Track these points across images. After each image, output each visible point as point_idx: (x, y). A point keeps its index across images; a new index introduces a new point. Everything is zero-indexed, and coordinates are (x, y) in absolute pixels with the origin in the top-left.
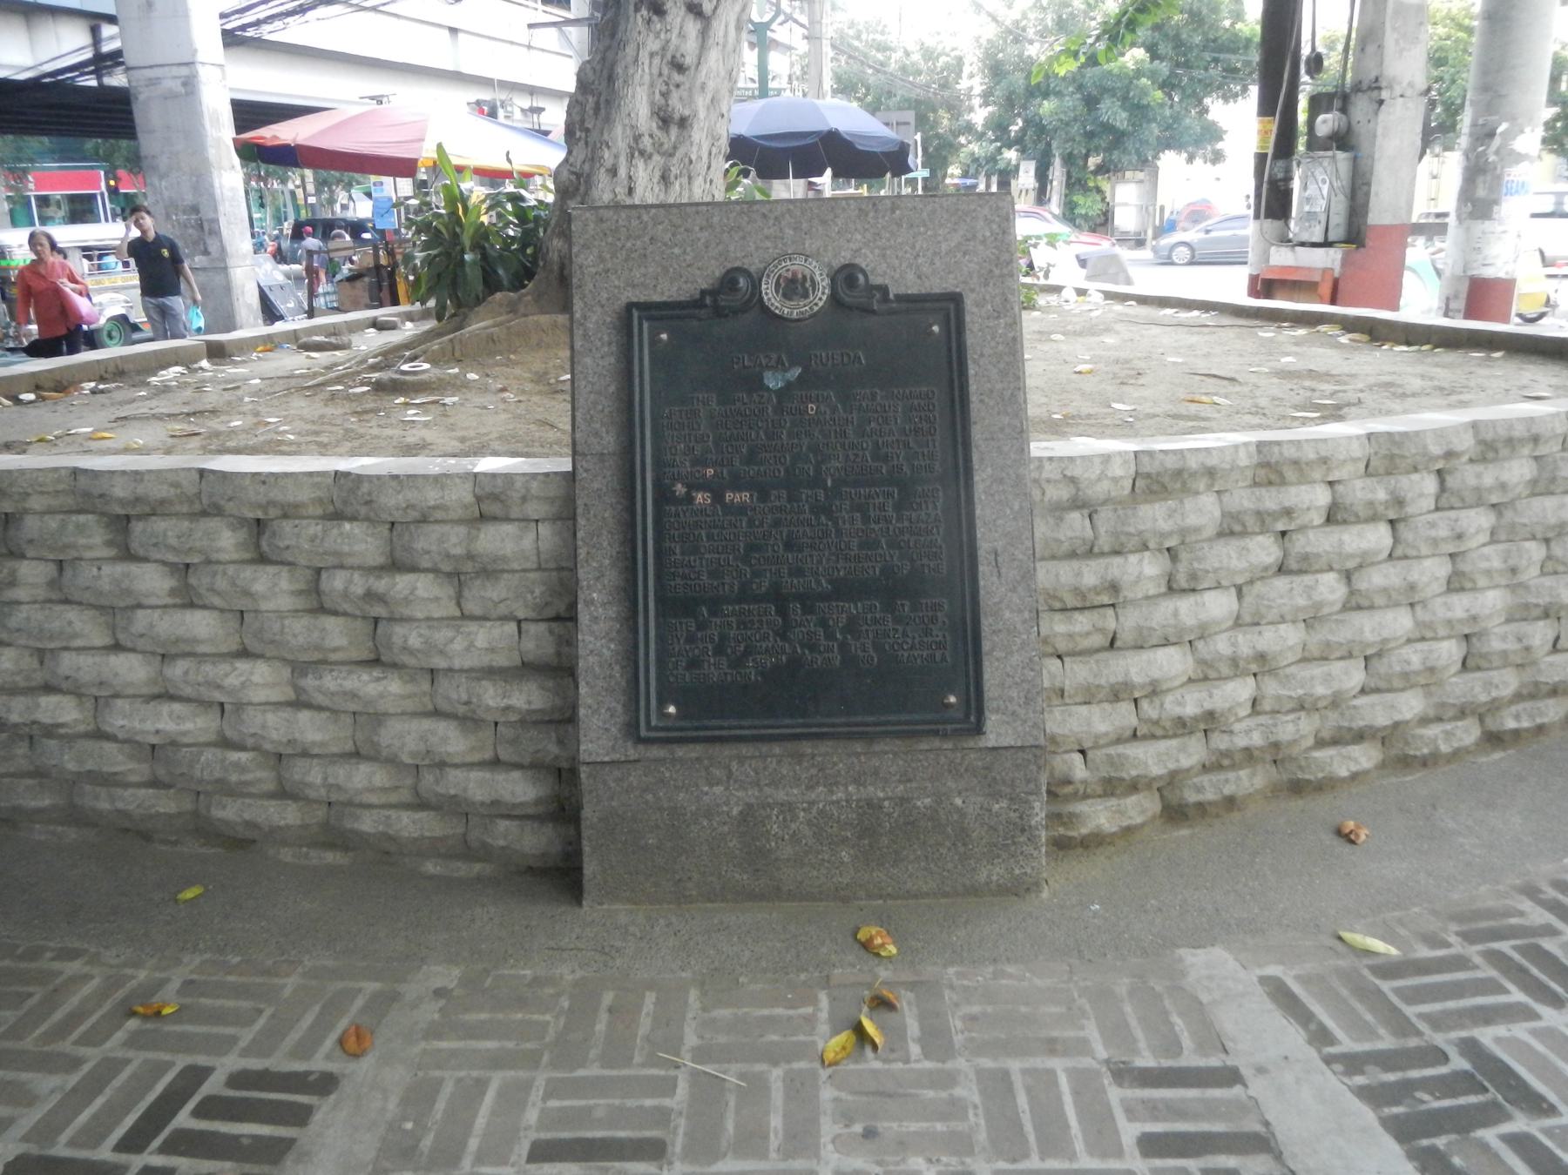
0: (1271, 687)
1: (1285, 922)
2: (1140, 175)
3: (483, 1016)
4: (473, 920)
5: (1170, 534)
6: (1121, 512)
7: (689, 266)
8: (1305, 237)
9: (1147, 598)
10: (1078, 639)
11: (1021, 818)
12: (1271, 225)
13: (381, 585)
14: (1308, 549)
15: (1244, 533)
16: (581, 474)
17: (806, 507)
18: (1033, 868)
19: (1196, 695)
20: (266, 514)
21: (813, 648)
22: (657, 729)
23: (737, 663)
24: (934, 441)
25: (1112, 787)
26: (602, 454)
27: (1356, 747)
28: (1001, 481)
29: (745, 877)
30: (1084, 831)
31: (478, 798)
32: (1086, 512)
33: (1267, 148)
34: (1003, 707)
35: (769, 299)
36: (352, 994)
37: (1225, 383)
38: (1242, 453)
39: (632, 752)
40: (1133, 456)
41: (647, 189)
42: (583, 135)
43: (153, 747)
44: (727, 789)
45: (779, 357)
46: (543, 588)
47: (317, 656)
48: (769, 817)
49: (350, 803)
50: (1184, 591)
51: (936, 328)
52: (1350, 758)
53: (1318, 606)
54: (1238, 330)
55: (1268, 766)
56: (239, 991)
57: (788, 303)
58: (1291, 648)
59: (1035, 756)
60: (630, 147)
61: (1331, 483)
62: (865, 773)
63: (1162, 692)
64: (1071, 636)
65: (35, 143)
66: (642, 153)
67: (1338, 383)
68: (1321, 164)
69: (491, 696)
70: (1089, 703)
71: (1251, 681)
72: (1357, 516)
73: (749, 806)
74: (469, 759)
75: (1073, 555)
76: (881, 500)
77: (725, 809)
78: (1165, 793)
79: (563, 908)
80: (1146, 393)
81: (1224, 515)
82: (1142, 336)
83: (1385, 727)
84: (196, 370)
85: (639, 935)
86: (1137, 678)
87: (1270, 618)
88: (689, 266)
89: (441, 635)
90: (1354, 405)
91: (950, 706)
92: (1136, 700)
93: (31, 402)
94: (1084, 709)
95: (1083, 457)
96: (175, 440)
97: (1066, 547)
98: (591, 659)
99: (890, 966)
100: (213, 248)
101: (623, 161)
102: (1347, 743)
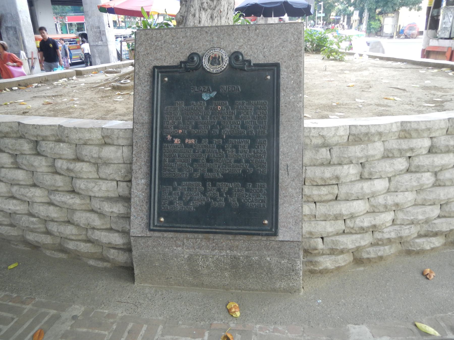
0: (401, 215)
1: (394, 315)
2: (393, 15)
3: (85, 330)
4: (96, 286)
5: (362, 158)
6: (342, 149)
7: (177, 52)
8: (443, 36)
9: (351, 182)
10: (322, 196)
11: (292, 266)
12: (431, 32)
13: (71, 166)
14: (419, 164)
15: (393, 157)
16: (135, 130)
17: (215, 146)
18: (297, 284)
19: (369, 219)
20: (37, 139)
21: (215, 199)
22: (156, 226)
24: (265, 121)
25: (333, 252)
26: (143, 123)
27: (434, 238)
28: (291, 138)
29: (191, 279)
30: (321, 268)
31: (104, 241)
32: (328, 149)
33: (431, 5)
36: (45, 314)
37: (402, 91)
38: (394, 126)
39: (149, 234)
40: (348, 127)
41: (205, 20)
42: (185, 3)
43: (10, 213)
44: (183, 248)
45: (209, 87)
46: (125, 170)
47: (54, 188)
48: (198, 259)
49: (66, 238)
50: (367, 179)
51: (269, 77)
52: (431, 242)
53: (422, 185)
54: (413, 70)
55: (397, 244)
56: (10, 309)
58: (409, 201)
59: (298, 245)
60: (200, 7)
61: (431, 138)
62: (233, 247)
63: (356, 217)
64: (320, 195)
65: (68, 8)
66: (204, 9)
67: (445, 92)
68: (450, 10)
69: (107, 208)
70: (326, 220)
71: (392, 213)
72: (441, 150)
73: (191, 255)
74: (102, 227)
75: (322, 165)
76: (244, 144)
77: (182, 255)
78: (355, 253)
79: (128, 284)
80: (371, 95)
81: (385, 150)
82: (377, 72)
83: (447, 231)
84: (70, 80)
85: (150, 298)
86: (344, 212)
87: (402, 189)
88: (177, 52)
89: (91, 185)
90: (449, 101)
91: (265, 224)
92: (345, 220)
93: (15, 90)
94: (323, 223)
95: (327, 128)
96: (43, 106)
97: (319, 162)
98: (136, 199)
99: (236, 322)
100: (104, 39)
101: (197, 11)
102: (431, 236)
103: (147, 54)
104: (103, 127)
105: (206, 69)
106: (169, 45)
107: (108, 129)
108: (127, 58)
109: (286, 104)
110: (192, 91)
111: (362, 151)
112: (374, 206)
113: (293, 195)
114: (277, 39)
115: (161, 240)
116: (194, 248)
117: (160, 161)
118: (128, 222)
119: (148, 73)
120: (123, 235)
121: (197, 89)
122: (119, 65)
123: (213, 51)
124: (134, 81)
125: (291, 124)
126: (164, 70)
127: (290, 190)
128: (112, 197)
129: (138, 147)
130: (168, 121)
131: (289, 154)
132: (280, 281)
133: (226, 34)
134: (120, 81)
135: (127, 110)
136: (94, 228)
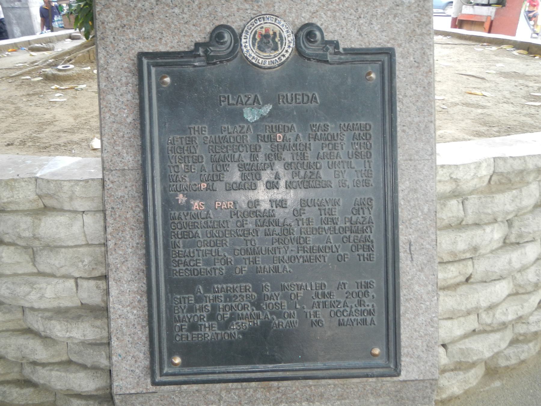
7: (186, 23)
16: (108, 183)
22: (167, 375)
23: (225, 326)
28: (415, 191)
31: (59, 387)
32: (460, 200)
34: (411, 353)
35: (248, 51)
37: (479, 80)
39: (152, 388)
40: (492, 160)
45: (256, 96)
46: (90, 259)
57: (262, 54)
62: (314, 396)
70: (452, 318)
76: (330, 207)
88: (186, 23)
89: (23, 290)
91: (375, 355)
95: (463, 165)
98: (120, 321)
103: (123, 27)
104: (38, 175)
105: (250, 58)
107: (48, 181)
108: (61, 26)
109: (405, 128)
110: (222, 103)
111: (513, 201)
112: (520, 286)
113: (421, 298)
115: (176, 396)
119: (128, 68)
120: (95, 374)
121: (233, 98)
122: (50, 38)
123: (262, 22)
124: (99, 82)
125: (415, 166)
126: (160, 61)
127: (417, 288)
128: (67, 307)
129: (118, 219)
130: (178, 166)
131: (412, 222)
134: (56, 65)
135: (75, 120)
136: (35, 363)
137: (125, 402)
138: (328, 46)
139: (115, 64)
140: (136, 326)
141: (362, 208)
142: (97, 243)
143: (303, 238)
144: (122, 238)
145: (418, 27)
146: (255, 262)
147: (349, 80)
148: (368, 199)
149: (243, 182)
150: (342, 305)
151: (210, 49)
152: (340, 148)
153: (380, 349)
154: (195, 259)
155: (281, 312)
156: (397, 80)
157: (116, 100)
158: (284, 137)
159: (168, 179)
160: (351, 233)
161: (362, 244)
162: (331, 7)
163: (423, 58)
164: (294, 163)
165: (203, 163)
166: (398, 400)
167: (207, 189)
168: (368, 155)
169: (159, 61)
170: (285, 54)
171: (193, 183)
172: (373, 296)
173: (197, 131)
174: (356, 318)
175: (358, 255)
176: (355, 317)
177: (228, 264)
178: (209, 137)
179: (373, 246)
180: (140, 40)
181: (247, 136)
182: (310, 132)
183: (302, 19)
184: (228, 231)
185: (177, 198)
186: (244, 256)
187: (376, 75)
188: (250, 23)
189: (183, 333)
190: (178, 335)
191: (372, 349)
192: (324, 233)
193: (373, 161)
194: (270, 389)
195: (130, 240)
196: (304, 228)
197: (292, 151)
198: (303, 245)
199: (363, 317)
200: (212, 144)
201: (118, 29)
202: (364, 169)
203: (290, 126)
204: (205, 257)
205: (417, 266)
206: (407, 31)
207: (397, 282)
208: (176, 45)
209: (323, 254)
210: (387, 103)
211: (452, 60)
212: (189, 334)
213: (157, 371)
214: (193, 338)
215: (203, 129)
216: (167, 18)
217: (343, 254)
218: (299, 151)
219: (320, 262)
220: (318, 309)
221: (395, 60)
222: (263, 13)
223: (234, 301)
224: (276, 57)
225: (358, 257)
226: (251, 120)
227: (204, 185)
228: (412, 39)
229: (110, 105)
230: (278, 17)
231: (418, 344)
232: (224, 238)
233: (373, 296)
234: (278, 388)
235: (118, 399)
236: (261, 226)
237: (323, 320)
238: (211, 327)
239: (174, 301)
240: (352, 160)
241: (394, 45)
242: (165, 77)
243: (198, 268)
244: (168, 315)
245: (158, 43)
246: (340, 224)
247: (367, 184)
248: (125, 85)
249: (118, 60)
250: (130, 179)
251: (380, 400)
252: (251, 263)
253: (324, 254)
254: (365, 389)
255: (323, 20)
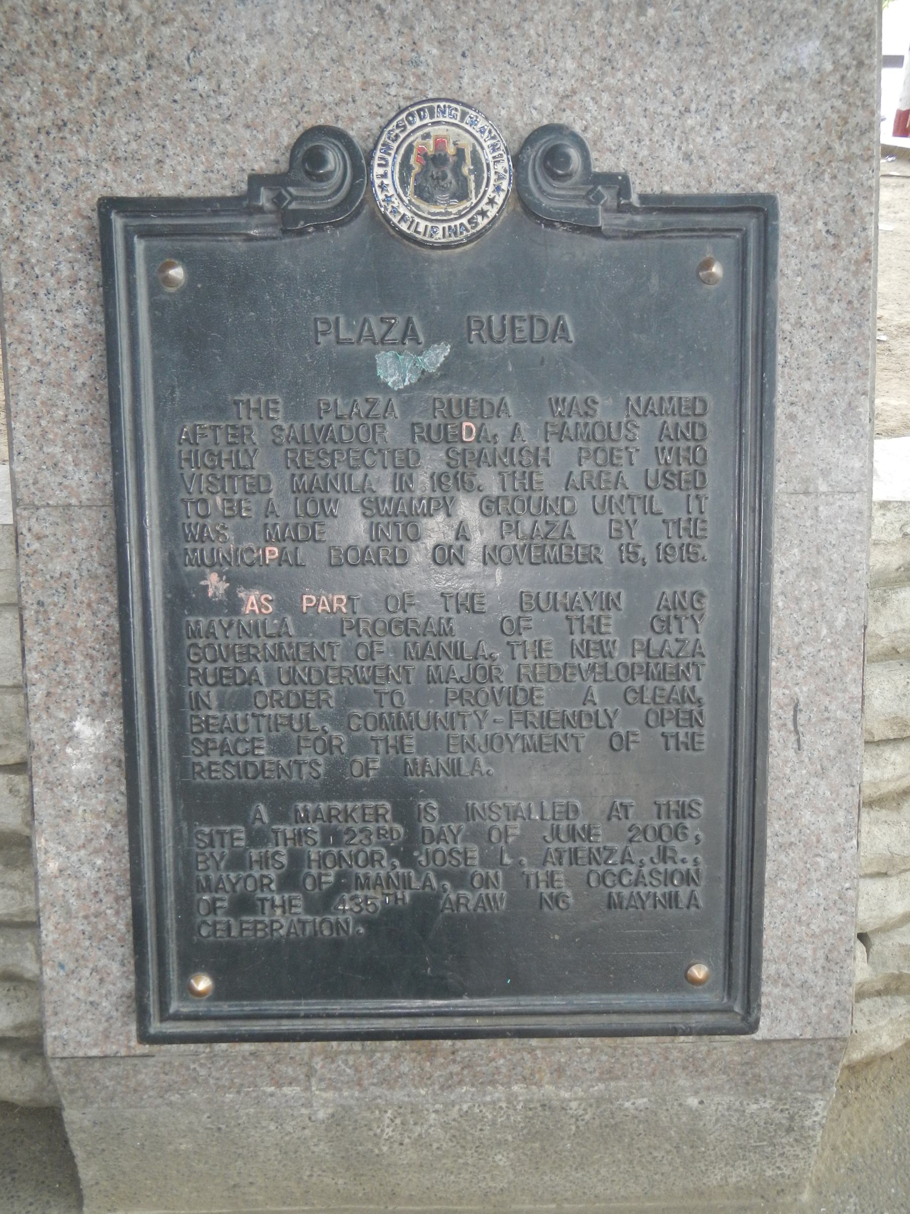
28: (815, 572)
39: (146, 1048)
45: (409, 321)
48: (379, 1120)
57: (427, 208)
70: (885, 875)
76: (596, 612)
91: (695, 982)
98: (60, 883)
103: (60, 129)
105: (395, 220)
106: (176, 78)
109: (794, 409)
114: (751, 61)
115: (201, 1065)
116: (360, 1085)
117: (176, 705)
118: (31, 947)
119: (74, 238)
120: (12, 993)
121: (349, 326)
123: (427, 120)
126: (158, 222)
129: (54, 632)
130: (204, 501)
131: (804, 653)
132: (727, 1164)
133: (484, 28)
137: (77, 1076)
138: (600, 188)
139: (40, 227)
140: (101, 895)
141: (676, 617)
142: (9, 683)
143: (523, 689)
144: (66, 680)
145: (840, 138)
146: (400, 747)
147: (655, 281)
148: (693, 594)
149: (375, 545)
150: (617, 858)
151: (290, 194)
152: (624, 461)
153: (709, 965)
154: (248, 737)
155: (464, 873)
156: (781, 282)
157: (45, 324)
158: (479, 431)
159: (181, 534)
160: (648, 679)
161: (673, 707)
162: (610, 80)
163: (849, 223)
164: (505, 498)
165: (271, 495)
166: (747, 1083)
167: (281, 561)
168: (697, 481)
169: (157, 221)
170: (486, 208)
171: (246, 545)
172: (697, 837)
173: (255, 410)
174: (652, 890)
175: (663, 734)
176: (649, 889)
177: (332, 753)
178: (285, 426)
179: (701, 714)
180: (105, 165)
181: (383, 427)
182: (549, 418)
183: (534, 113)
184: (333, 669)
185: (203, 583)
186: (373, 734)
187: (725, 270)
188: (395, 123)
189: (218, 919)
190: (204, 922)
191: (690, 966)
192: (578, 678)
193: (710, 496)
194: (432, 1055)
195: (86, 684)
196: (527, 666)
197: (500, 468)
198: (523, 709)
199: (670, 888)
200: (293, 445)
201: (48, 133)
202: (684, 517)
203: (496, 400)
204: (274, 734)
205: (811, 764)
206: (810, 150)
207: (758, 804)
208: (199, 180)
209: (574, 731)
210: (750, 344)
211: (898, 216)
212: (232, 921)
213: (153, 1009)
214: (242, 930)
215: (271, 406)
216: (177, 107)
217: (623, 733)
218: (519, 469)
219: (566, 750)
220: (557, 868)
221: (776, 229)
222: (431, 96)
223: (348, 844)
224: (461, 217)
225: (662, 740)
226: (394, 383)
227: (272, 552)
228: (823, 173)
229: (29, 337)
230: (470, 107)
231: (805, 955)
232: (323, 686)
233: (697, 837)
234: (453, 1053)
235: (58, 1068)
236: (418, 659)
237: (569, 893)
238: (286, 906)
239: (195, 841)
240: (655, 493)
241: (773, 187)
242: (172, 266)
243: (258, 761)
244: (182, 874)
245: (154, 174)
246: (620, 656)
247: (690, 555)
248: (67, 285)
249: (49, 218)
250: (85, 530)
251: (705, 1081)
252: (391, 751)
253: (576, 731)
254: (667, 1059)
255: (588, 116)
